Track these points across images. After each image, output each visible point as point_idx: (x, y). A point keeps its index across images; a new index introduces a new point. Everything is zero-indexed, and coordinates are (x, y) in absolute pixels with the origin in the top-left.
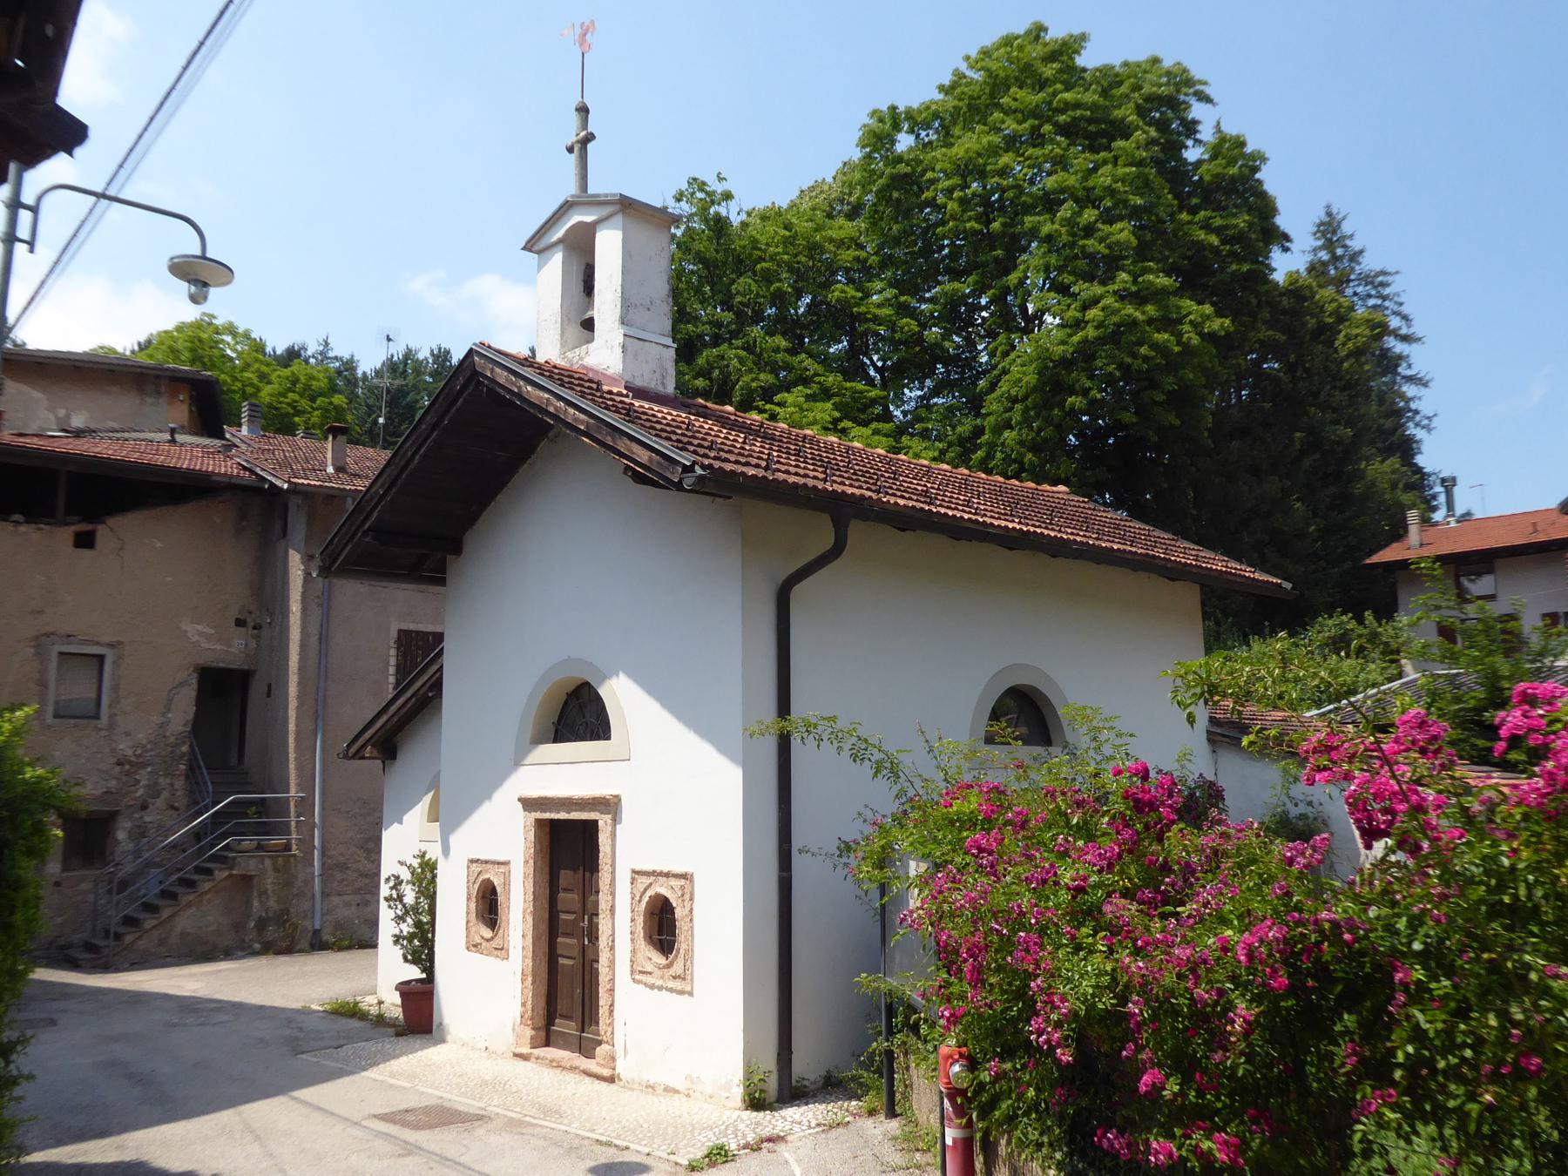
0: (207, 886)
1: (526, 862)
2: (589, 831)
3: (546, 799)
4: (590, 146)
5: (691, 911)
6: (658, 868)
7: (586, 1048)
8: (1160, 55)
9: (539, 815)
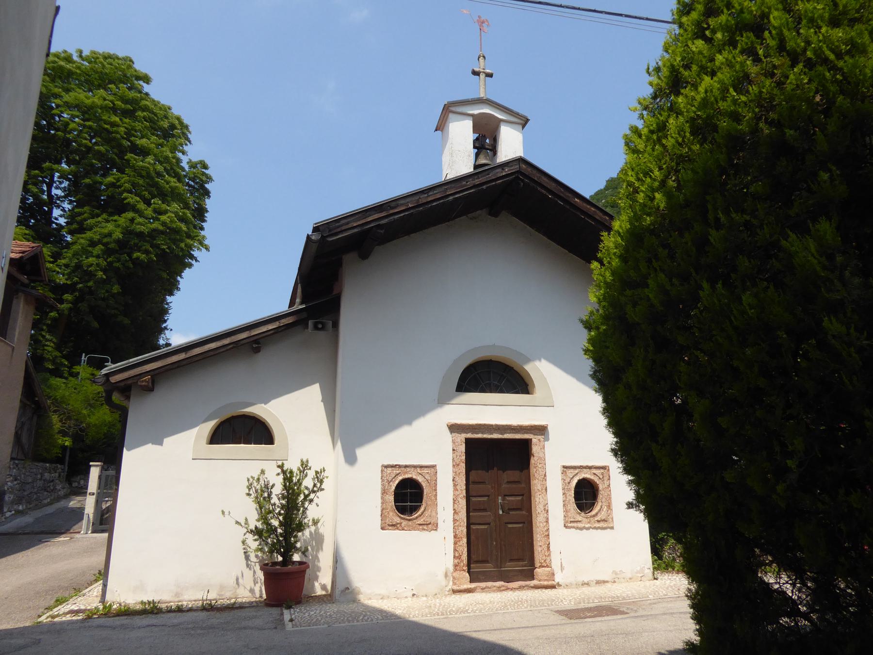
2: (526, 445)
3: (480, 425)
5: (609, 486)
7: (529, 574)
8: (622, 133)
9: (464, 436)
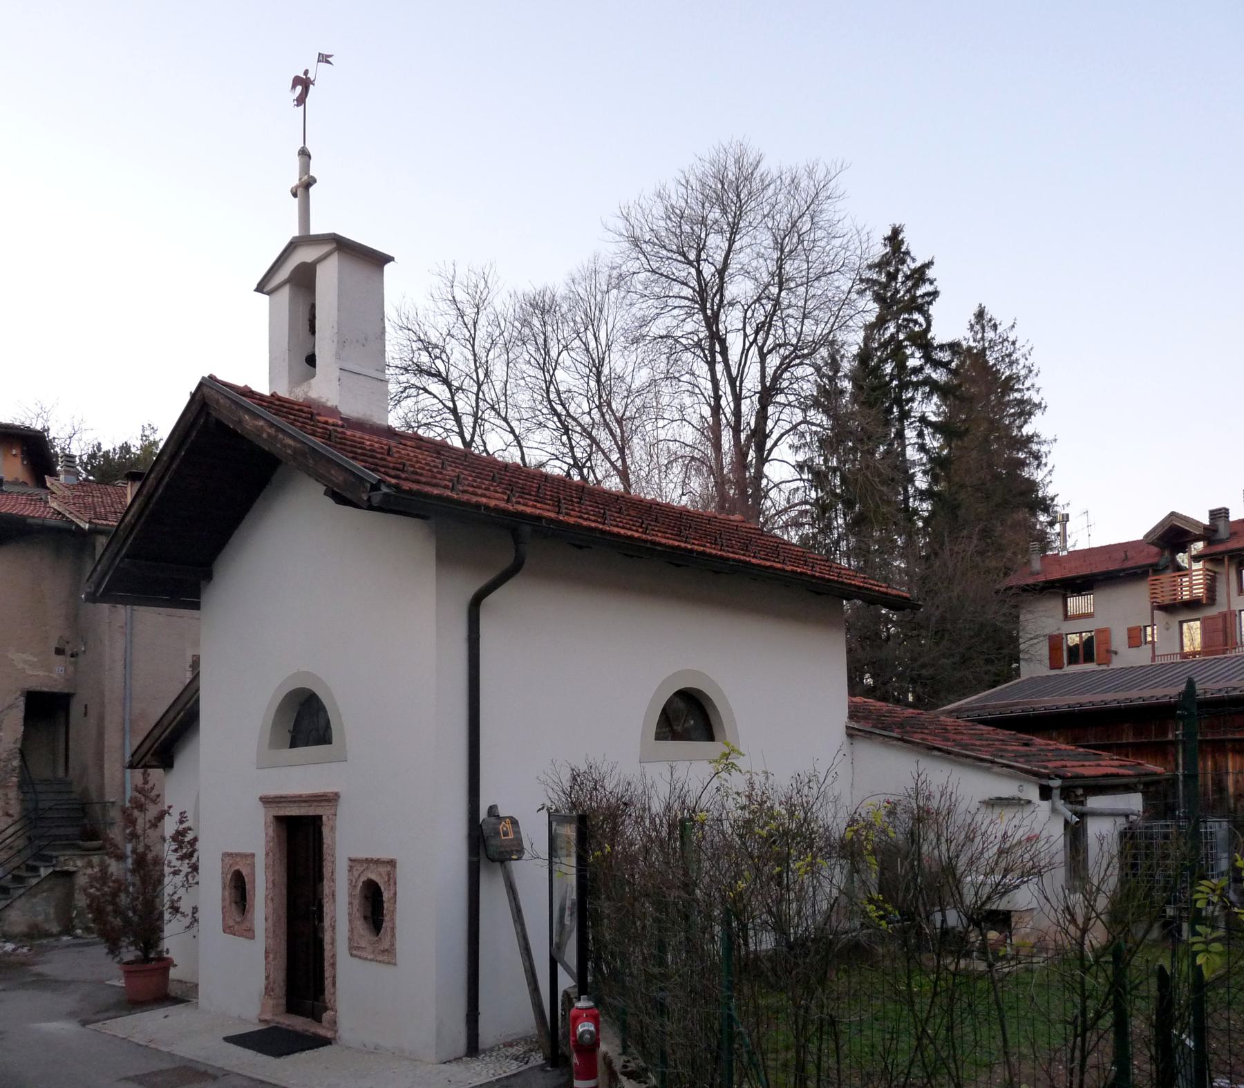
0: (34, 881)
1: (267, 855)
2: (315, 823)
4: (311, 190)
5: (395, 894)
6: (376, 856)
